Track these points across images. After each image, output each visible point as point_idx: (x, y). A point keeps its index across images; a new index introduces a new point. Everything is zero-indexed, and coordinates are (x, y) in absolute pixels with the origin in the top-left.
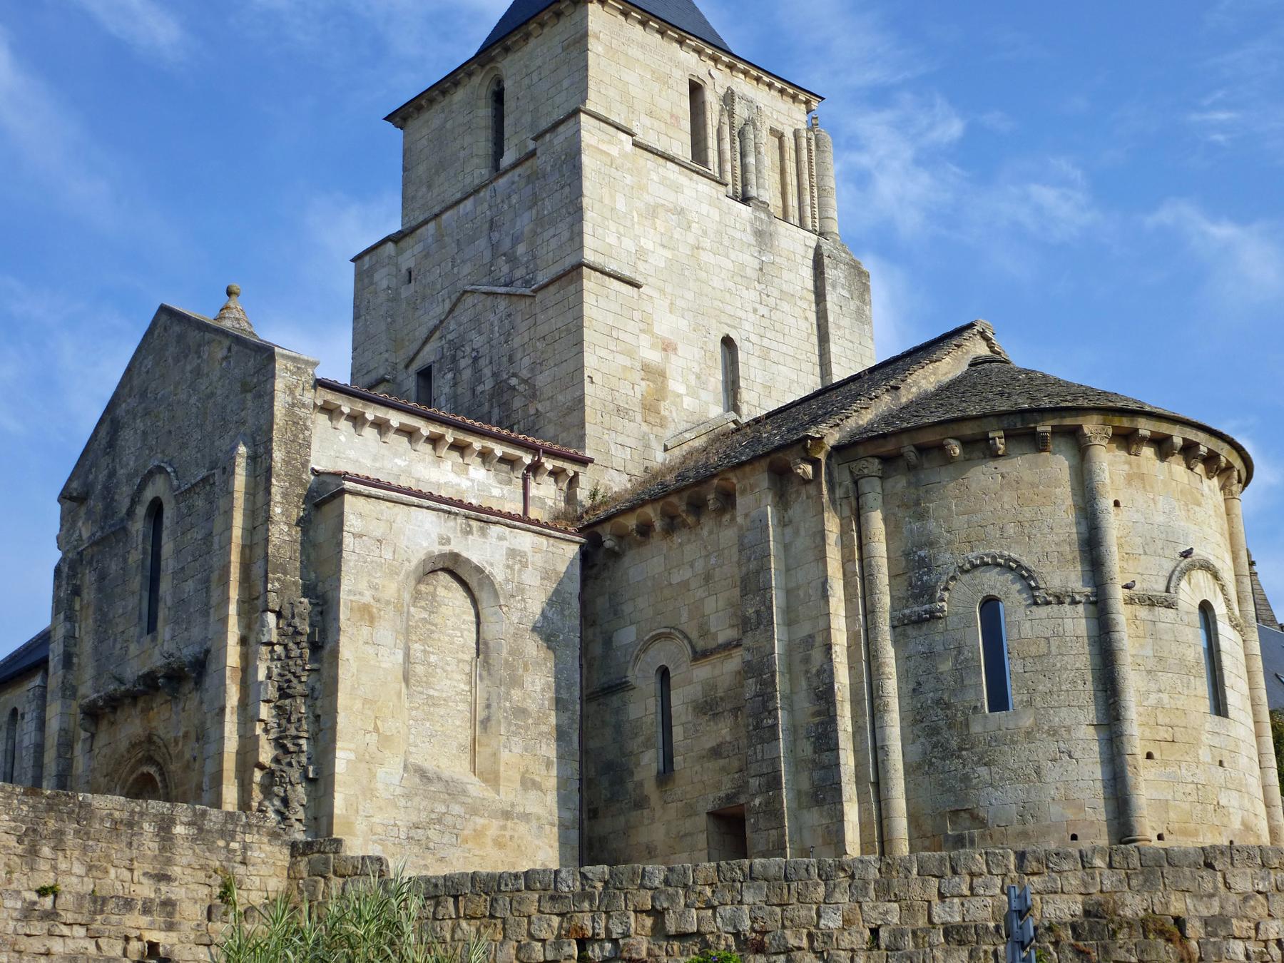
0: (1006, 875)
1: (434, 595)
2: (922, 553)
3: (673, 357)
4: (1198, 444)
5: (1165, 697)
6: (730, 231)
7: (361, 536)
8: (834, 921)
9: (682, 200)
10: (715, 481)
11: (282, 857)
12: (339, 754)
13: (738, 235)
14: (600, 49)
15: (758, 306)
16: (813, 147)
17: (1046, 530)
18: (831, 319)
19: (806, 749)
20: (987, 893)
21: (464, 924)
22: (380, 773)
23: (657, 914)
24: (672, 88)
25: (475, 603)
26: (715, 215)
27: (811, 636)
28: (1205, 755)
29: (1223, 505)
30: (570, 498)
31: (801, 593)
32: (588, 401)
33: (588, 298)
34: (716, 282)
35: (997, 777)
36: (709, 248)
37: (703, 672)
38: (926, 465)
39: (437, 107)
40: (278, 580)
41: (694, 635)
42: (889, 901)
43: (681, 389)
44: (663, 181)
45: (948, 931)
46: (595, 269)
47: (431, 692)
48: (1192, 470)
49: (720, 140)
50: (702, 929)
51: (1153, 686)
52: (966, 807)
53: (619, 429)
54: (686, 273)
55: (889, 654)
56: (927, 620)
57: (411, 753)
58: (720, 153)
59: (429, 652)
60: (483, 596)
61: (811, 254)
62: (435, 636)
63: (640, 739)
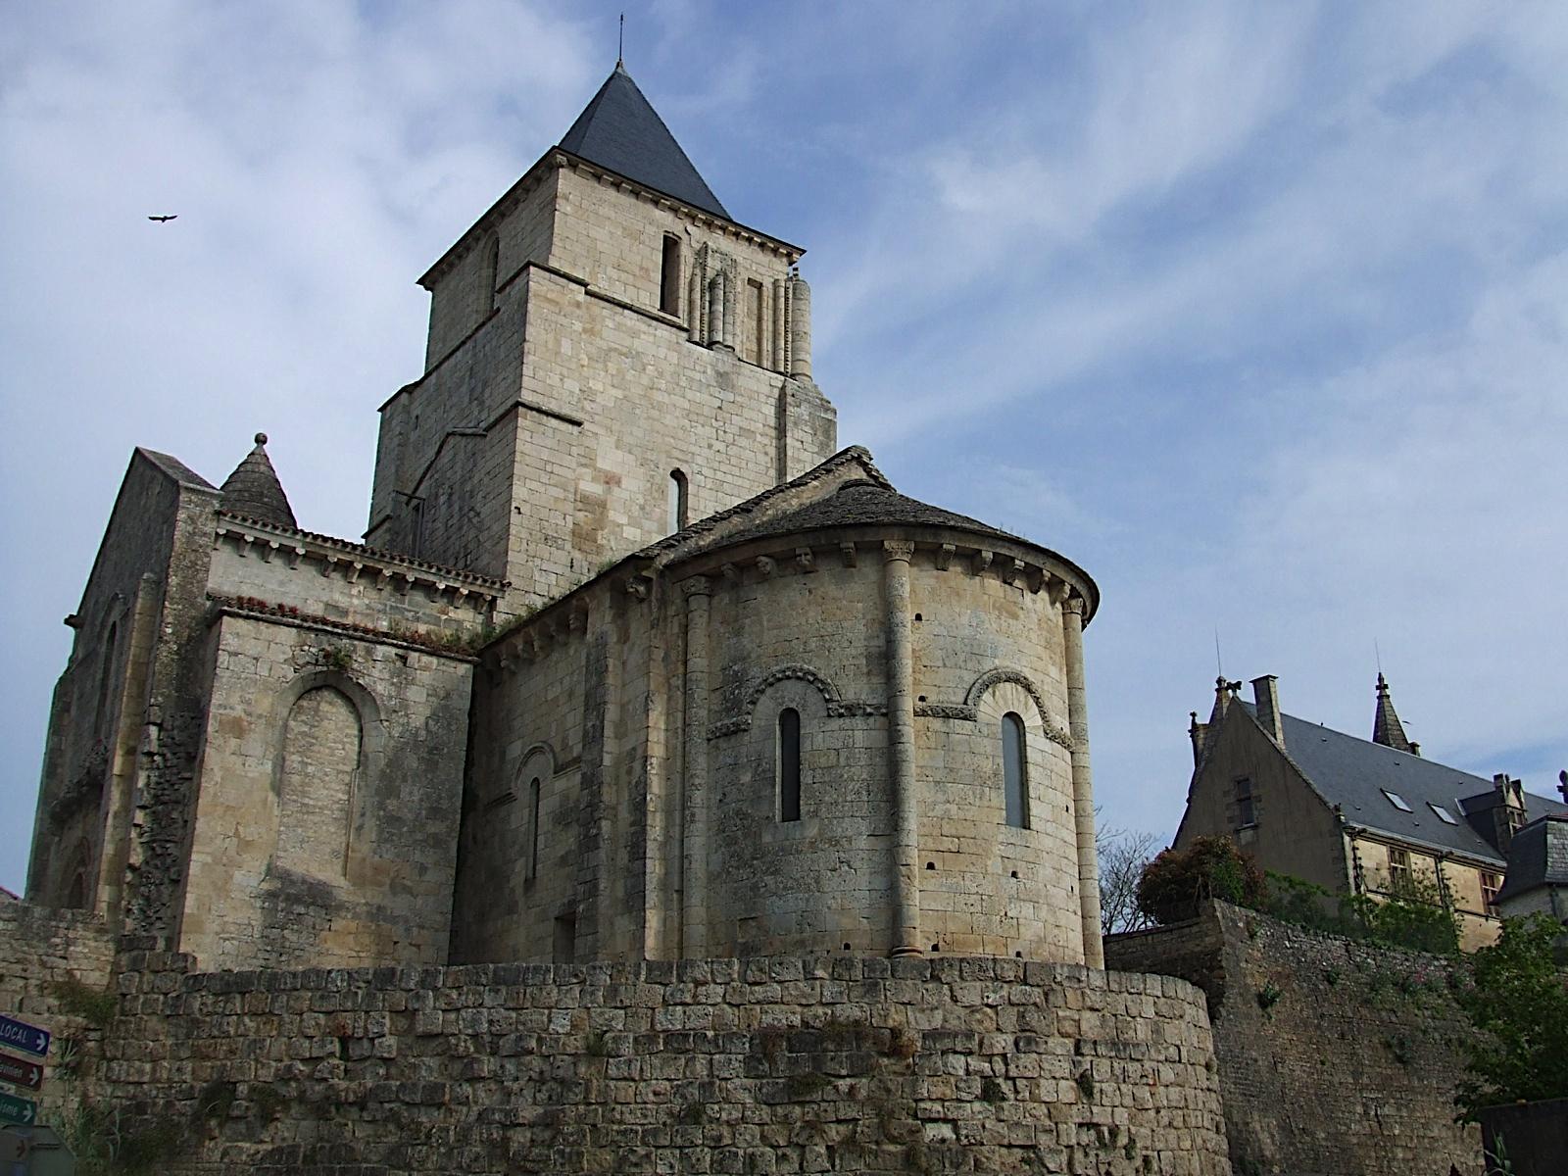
0: (729, 984)
1: (317, 710)
2: (736, 668)
3: (616, 490)
4: (1013, 559)
5: (954, 808)
6: (689, 373)
7: (236, 654)
8: (563, 1026)
9: (638, 344)
10: (574, 602)
11: (107, 953)
12: (194, 857)
13: (697, 376)
14: (569, 208)
15: (714, 442)
16: (791, 296)
17: (846, 644)
18: (789, 453)
19: (623, 857)
20: (709, 1002)
21: (247, 1020)
22: (238, 875)
23: (410, 1014)
24: (643, 243)
25: (359, 718)
26: (674, 357)
27: (634, 749)
28: (994, 865)
29: (1061, 619)
30: (489, 621)
31: (631, 708)
32: (513, 530)
33: (522, 435)
34: (669, 420)
35: (781, 886)
36: (663, 387)
37: (561, 784)
38: (746, 583)
39: (455, 271)
40: (162, 694)
41: (557, 749)
42: (616, 1008)
43: (624, 520)
44: (618, 327)
45: (669, 1035)
46: (532, 409)
47: (306, 801)
48: (1011, 584)
49: (691, 291)
50: (445, 1031)
51: (941, 797)
52: (753, 915)
53: (546, 556)
54: (637, 411)
55: (701, 763)
56: (735, 733)
57: (278, 857)
58: (691, 302)
59: (307, 763)
60: (366, 711)
61: (776, 393)
62: (315, 748)
63: (517, 847)
